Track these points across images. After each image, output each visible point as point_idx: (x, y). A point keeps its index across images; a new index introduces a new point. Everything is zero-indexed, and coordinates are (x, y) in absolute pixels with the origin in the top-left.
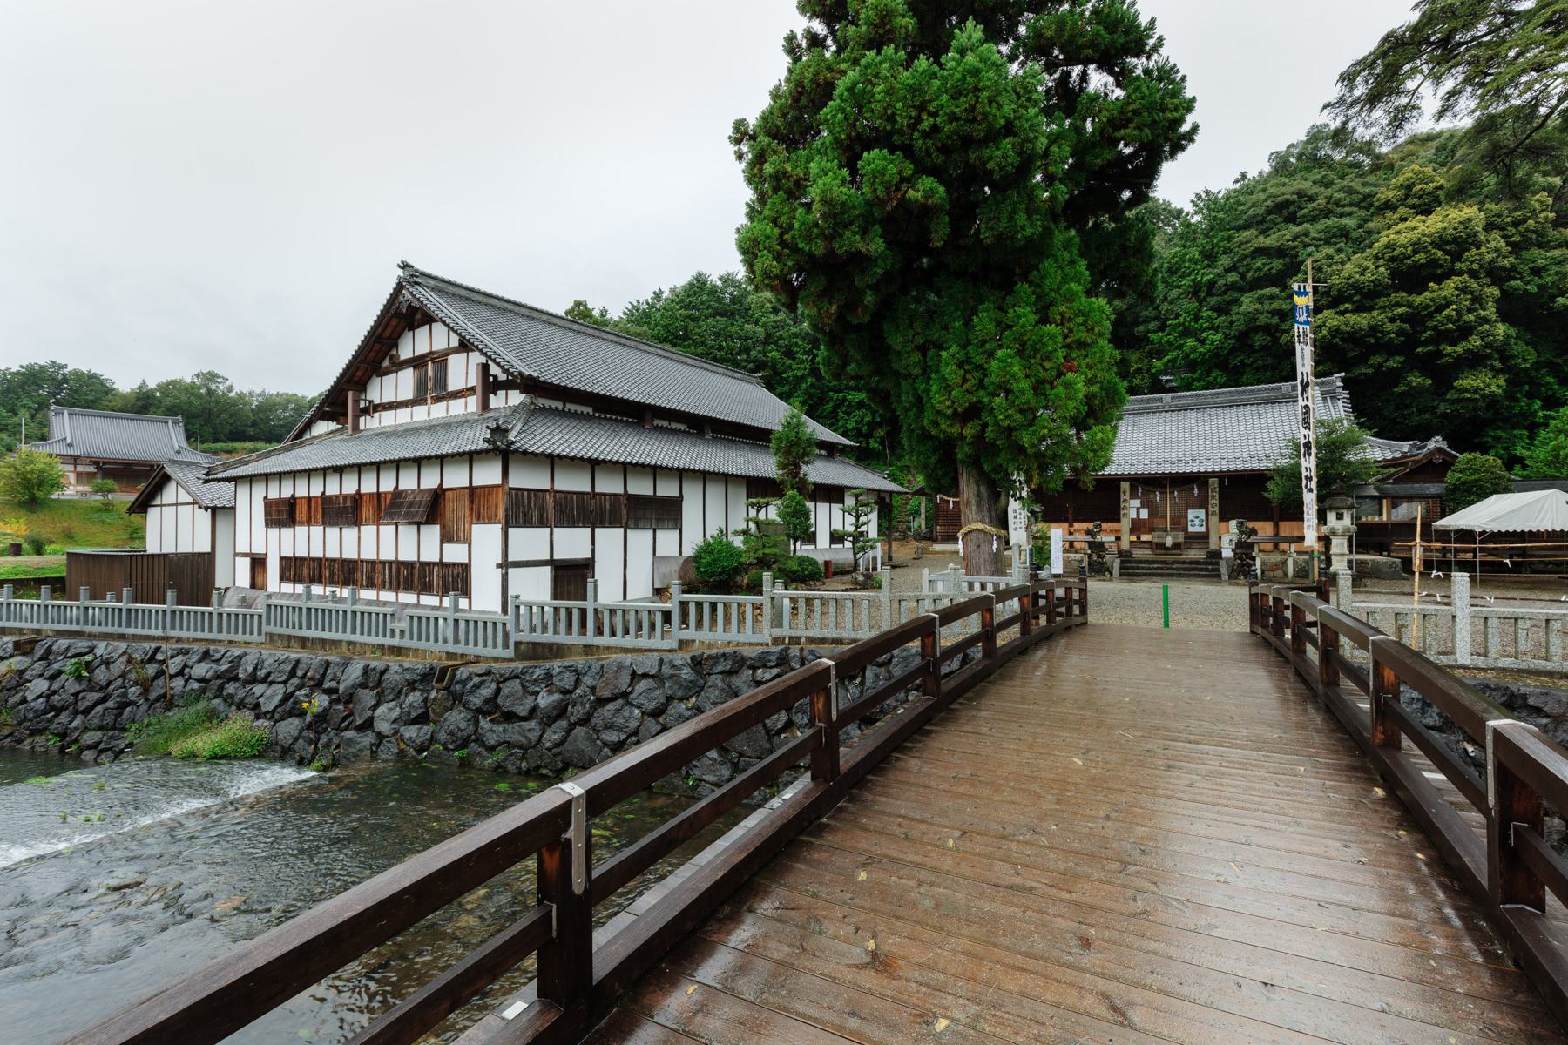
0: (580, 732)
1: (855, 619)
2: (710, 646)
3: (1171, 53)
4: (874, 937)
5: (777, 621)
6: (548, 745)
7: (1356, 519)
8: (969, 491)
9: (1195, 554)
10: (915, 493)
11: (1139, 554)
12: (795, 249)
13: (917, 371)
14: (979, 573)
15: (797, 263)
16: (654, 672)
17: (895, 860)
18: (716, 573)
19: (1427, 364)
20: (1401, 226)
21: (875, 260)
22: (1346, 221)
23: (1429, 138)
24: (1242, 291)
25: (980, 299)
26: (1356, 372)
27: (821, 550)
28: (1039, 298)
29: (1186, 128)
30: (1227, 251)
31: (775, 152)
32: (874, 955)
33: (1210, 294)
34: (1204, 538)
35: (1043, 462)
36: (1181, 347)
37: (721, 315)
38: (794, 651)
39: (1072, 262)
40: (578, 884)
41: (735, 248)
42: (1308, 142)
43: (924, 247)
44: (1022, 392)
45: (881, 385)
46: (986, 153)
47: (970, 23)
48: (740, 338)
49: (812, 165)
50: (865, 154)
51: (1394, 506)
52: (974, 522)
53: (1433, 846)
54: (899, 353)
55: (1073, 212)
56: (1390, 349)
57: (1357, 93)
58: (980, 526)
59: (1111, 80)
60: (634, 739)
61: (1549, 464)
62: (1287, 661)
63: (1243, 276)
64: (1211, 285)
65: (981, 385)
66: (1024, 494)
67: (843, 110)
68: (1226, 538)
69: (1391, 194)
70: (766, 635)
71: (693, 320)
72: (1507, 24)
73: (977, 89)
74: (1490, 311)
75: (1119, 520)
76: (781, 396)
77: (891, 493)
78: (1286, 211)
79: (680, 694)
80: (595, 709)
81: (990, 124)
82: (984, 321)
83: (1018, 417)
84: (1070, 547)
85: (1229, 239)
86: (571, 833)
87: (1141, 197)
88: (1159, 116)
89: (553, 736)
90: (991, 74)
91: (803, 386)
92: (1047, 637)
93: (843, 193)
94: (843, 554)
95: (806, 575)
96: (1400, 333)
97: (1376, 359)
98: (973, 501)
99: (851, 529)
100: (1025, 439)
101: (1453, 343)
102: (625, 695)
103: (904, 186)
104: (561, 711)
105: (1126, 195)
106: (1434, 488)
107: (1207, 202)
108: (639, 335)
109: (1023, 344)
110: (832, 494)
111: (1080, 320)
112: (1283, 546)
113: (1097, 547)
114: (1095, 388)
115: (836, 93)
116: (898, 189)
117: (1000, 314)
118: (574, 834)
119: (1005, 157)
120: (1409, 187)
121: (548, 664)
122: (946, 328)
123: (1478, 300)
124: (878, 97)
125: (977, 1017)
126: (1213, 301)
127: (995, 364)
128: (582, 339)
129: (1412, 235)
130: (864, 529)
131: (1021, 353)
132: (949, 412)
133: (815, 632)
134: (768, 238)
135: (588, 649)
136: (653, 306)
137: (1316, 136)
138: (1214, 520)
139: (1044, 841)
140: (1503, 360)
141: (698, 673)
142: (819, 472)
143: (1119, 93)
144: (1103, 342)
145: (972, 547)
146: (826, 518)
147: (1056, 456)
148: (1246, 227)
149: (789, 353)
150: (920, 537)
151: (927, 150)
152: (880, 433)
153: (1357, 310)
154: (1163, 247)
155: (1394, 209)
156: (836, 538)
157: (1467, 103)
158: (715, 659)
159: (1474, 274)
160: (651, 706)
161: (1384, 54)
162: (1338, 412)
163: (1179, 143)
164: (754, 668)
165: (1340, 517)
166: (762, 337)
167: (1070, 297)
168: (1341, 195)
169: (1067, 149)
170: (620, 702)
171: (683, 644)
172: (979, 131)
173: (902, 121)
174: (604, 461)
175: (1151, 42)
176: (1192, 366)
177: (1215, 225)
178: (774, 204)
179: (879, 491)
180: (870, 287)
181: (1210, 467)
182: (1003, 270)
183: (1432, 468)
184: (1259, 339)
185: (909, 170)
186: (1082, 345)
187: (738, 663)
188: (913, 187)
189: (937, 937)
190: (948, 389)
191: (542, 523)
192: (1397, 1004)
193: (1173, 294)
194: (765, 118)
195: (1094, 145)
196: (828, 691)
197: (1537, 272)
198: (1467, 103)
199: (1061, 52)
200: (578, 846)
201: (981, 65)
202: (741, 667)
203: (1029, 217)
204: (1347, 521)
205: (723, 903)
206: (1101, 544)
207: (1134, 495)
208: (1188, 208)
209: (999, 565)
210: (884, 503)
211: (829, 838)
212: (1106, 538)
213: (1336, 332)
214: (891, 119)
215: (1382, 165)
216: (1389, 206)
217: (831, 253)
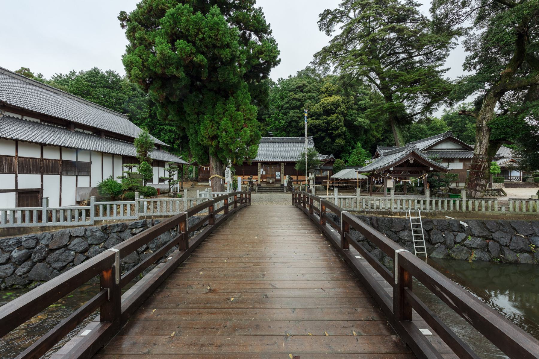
0: (40, 265)
1: (174, 208)
2: (110, 222)
3: (275, 35)
4: (209, 285)
5: (141, 210)
6: (19, 274)
7: (315, 175)
8: (213, 163)
9: (278, 185)
10: (192, 164)
11: (263, 185)
12: (149, 69)
13: (195, 121)
14: (216, 191)
15: (150, 74)
16: (82, 235)
17: (210, 268)
18: (111, 193)
19: (330, 135)
20: (326, 98)
21: (181, 80)
22: (314, 94)
23: (331, 76)
24: (290, 109)
25: (217, 100)
26: (317, 135)
27: (155, 184)
28: (236, 102)
29: (278, 59)
30: (286, 97)
31: (140, 29)
32: (210, 290)
33: (282, 109)
34: (280, 180)
35: (237, 155)
36: (274, 124)
37: (107, 87)
38: (149, 221)
39: (246, 93)
40: (117, 281)
41: (122, 63)
42: (306, 70)
43: (199, 79)
44: (231, 132)
45: (182, 125)
46: (221, 52)
47: (216, 6)
48: (116, 99)
49: (156, 39)
50: (178, 41)
51: (323, 172)
52: (215, 175)
53: (332, 243)
54: (189, 114)
55: (247, 77)
56: (323, 131)
57: (317, 61)
58: (217, 176)
59: (258, 38)
60: (71, 264)
61: (352, 162)
62: (302, 210)
63: (290, 105)
64: (282, 106)
65: (218, 128)
66: (230, 166)
67: (169, 22)
68: (285, 180)
69: (323, 89)
70: (136, 215)
71: (92, 87)
72: (347, 53)
73: (218, 29)
74: (342, 124)
75: (257, 175)
76: (136, 124)
77: (183, 164)
78: (300, 88)
79: (96, 242)
80: (48, 254)
81: (222, 42)
82: (219, 107)
83: (230, 140)
84: (243, 183)
85: (287, 94)
86: (115, 264)
87: (265, 77)
88: (271, 54)
89: (21, 270)
90: (223, 26)
91: (146, 121)
92: (241, 209)
93: (169, 52)
94: (165, 186)
95: (151, 193)
96: (325, 126)
97: (320, 133)
98: (214, 167)
99: (168, 177)
100: (232, 147)
101: (335, 131)
102: (66, 246)
103: (192, 56)
104: (28, 257)
105: (261, 75)
106: (331, 168)
107: (281, 81)
108: (62, 89)
109: (232, 117)
110: (160, 163)
111: (249, 111)
112: (299, 182)
113: (251, 183)
114: (253, 133)
115: (166, 14)
116: (190, 56)
117: (224, 106)
118: (116, 264)
119: (227, 54)
120: (327, 88)
121: (18, 237)
122: (206, 108)
123: (340, 120)
124: (183, 21)
125: (241, 295)
126: (283, 111)
127: (223, 122)
128: (31, 87)
129: (328, 101)
130: (172, 177)
131: (231, 119)
132: (207, 137)
133: (156, 214)
134: (137, 62)
135: (43, 228)
136: (70, 78)
137: (308, 69)
138: (283, 175)
139: (250, 256)
140: (345, 136)
141: (104, 233)
142: (154, 155)
143: (260, 43)
144: (255, 119)
145: (214, 183)
146: (158, 173)
147: (241, 153)
148: (291, 91)
149: (139, 107)
150: (192, 180)
151: (201, 45)
152: (178, 142)
153: (316, 119)
154: (271, 94)
155: (324, 94)
156: (161, 180)
157: (339, 71)
158: (113, 227)
159: (339, 114)
160: (81, 249)
161: (323, 52)
162: (311, 146)
163: (276, 63)
164: (132, 229)
165: (312, 175)
166: (127, 99)
167: (246, 104)
168: (312, 87)
169: (245, 57)
170: (63, 249)
171: (96, 222)
172: (219, 44)
173: (192, 32)
174: (49, 144)
175: (269, 30)
176: (277, 129)
177: (284, 89)
178: (140, 50)
179: (178, 163)
180: (178, 89)
181: (282, 160)
182: (225, 92)
183: (330, 162)
184: (294, 124)
185: (194, 51)
186: (249, 119)
187: (123, 228)
188: (196, 57)
189: (227, 282)
190: (207, 129)
191: (10, 172)
192: (326, 272)
193: (273, 107)
194: (135, 14)
195: (253, 58)
196: (185, 221)
197: (351, 115)
198: (339, 71)
199: (244, 24)
200: (117, 269)
201: (219, 22)
202: (125, 229)
203: (234, 76)
204: (313, 176)
205: (157, 288)
206: (252, 182)
207: (262, 168)
208: (277, 82)
209: (223, 189)
210: (180, 167)
211: (187, 266)
212: (254, 180)
213: (311, 124)
214: (188, 30)
215: (321, 81)
216: (323, 93)
217: (164, 74)
